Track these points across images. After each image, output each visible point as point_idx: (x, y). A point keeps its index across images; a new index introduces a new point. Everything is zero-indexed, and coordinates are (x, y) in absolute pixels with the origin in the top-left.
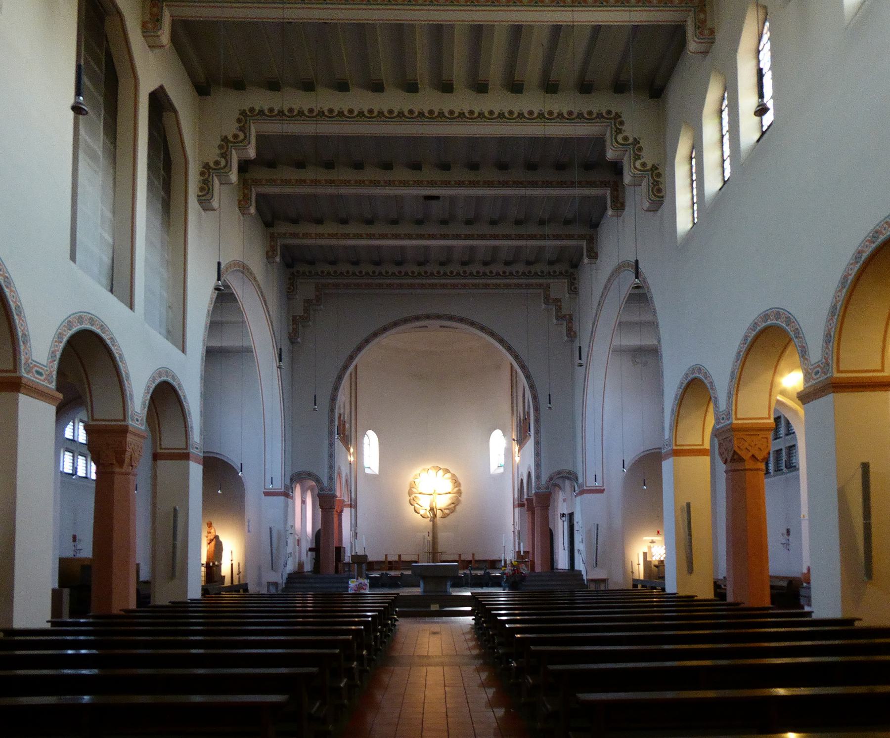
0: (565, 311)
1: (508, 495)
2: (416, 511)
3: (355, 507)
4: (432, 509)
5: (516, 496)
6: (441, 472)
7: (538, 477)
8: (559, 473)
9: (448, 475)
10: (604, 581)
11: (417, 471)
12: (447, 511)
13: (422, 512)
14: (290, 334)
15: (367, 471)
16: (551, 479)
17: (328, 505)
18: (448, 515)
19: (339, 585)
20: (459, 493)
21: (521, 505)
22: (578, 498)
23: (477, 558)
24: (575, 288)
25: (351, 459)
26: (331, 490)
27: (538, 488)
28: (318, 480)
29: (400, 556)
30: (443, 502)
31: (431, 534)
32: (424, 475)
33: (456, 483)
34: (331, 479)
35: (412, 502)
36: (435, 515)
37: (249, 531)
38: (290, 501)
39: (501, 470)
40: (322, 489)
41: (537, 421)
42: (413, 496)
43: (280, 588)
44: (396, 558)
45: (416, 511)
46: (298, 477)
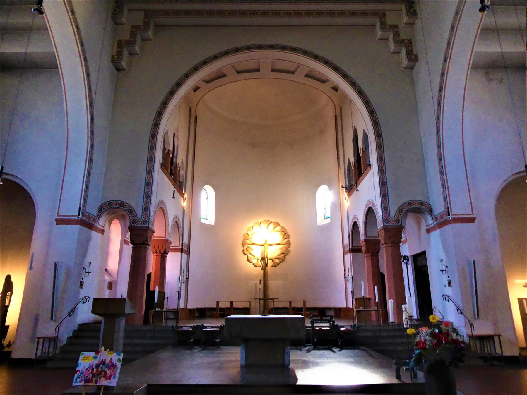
0: (403, 36)
1: (339, 240)
2: (248, 261)
3: (188, 253)
4: (263, 259)
5: (347, 241)
6: (272, 226)
7: (385, 209)
8: (410, 204)
9: (278, 228)
10: (489, 338)
11: (251, 224)
12: (277, 261)
13: (254, 261)
14: (113, 57)
15: (203, 221)
16: (400, 210)
17: (139, 237)
18: (278, 264)
19: (139, 341)
20: (289, 243)
21: (354, 250)
22: (436, 234)
23: (308, 305)
24: (415, 11)
25: (184, 204)
26: (145, 222)
27: (386, 220)
28: (131, 211)
29: (232, 303)
30: (273, 252)
31: (262, 282)
32: (256, 228)
33: (286, 235)
34: (146, 209)
35: (246, 252)
36: (266, 264)
37: (31, 268)
38: (95, 235)
39: (328, 221)
40: (134, 222)
41: (380, 147)
42: (246, 247)
43: (60, 344)
44: (228, 305)
45: (248, 261)
46: (114, 208)
